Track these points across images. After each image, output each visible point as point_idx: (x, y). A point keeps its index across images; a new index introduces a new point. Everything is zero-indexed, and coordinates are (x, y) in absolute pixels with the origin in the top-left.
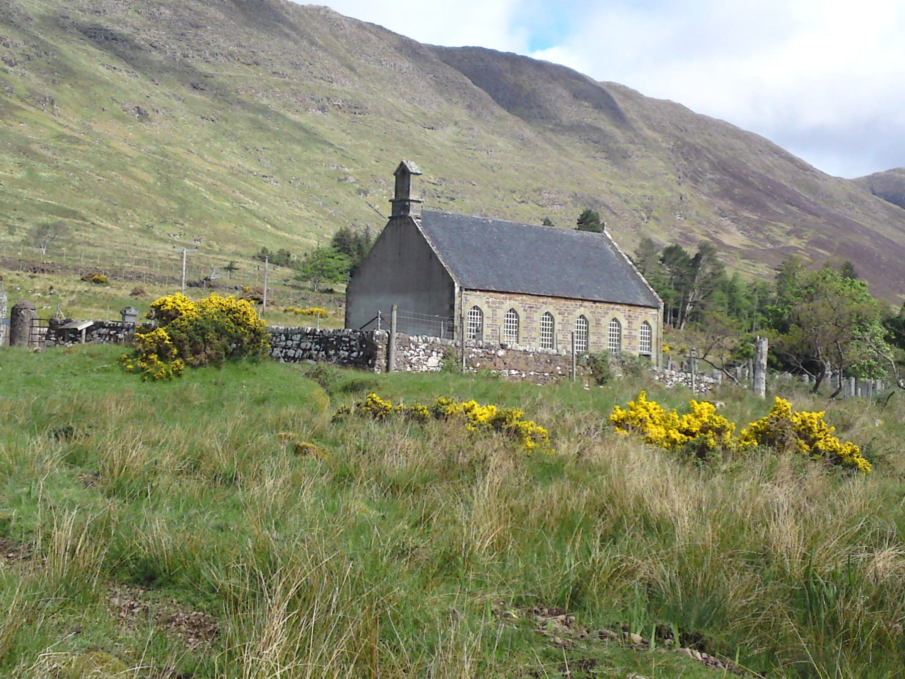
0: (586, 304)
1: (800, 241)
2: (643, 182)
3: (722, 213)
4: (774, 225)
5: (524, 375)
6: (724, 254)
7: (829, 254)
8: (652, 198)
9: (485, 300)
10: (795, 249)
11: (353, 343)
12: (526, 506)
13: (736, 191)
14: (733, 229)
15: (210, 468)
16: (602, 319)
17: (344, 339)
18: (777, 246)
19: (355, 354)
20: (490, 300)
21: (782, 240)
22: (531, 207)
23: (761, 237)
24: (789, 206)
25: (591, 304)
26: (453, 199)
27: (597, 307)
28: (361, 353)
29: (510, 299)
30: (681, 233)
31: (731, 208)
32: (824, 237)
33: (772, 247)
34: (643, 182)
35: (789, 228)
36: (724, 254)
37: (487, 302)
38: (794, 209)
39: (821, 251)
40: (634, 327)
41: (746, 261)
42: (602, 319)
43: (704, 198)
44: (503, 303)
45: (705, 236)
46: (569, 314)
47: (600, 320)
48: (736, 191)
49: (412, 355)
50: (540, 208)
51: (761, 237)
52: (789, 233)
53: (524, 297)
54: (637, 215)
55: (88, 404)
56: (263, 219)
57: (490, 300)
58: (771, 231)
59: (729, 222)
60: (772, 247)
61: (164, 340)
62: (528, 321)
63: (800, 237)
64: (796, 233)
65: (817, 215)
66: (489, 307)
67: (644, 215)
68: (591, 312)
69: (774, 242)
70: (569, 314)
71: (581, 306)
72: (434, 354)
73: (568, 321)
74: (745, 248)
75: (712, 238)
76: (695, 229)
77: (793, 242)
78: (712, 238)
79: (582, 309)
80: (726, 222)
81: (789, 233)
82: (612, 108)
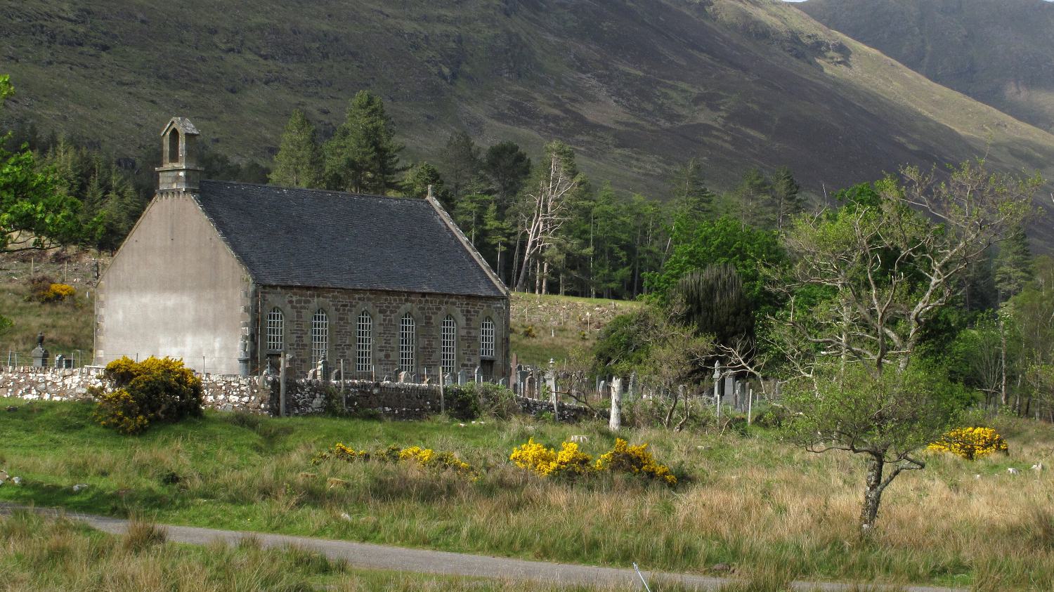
1: (715, 115)
2: (442, 12)
3: (582, 65)
4: (671, 87)
5: (397, 412)
6: (586, 138)
7: (763, 137)
8: (459, 40)
9: (287, 298)
10: (707, 129)
11: (243, 388)
13: (606, 25)
14: (603, 94)
15: (1024, 427)
17: (233, 384)
18: (678, 124)
19: (246, 399)
20: (294, 299)
21: (684, 112)
22: (248, 61)
23: (650, 107)
24: (695, 53)
26: (105, 48)
28: (253, 398)
30: (512, 102)
31: (598, 57)
32: (756, 107)
33: (668, 125)
34: (442, 12)
35: (695, 91)
36: (586, 138)
37: (291, 302)
38: (704, 57)
39: (752, 133)
41: (627, 152)
43: (551, 38)
44: (309, 302)
45: (555, 106)
47: (430, 318)
48: (606, 25)
49: (298, 398)
50: (261, 61)
51: (650, 107)
52: (697, 100)
54: (434, 70)
57: (294, 299)
58: (666, 96)
59: (594, 82)
60: (668, 125)
61: (128, 400)
62: (342, 323)
63: (715, 108)
64: (710, 101)
65: (745, 70)
66: (293, 307)
67: (446, 71)
68: (420, 309)
69: (672, 117)
70: (392, 312)
71: (407, 300)
72: (318, 395)
73: (390, 320)
74: (621, 128)
75: (567, 111)
76: (536, 95)
77: (704, 116)
78: (567, 111)
79: (409, 304)
80: (589, 81)
81: (697, 100)
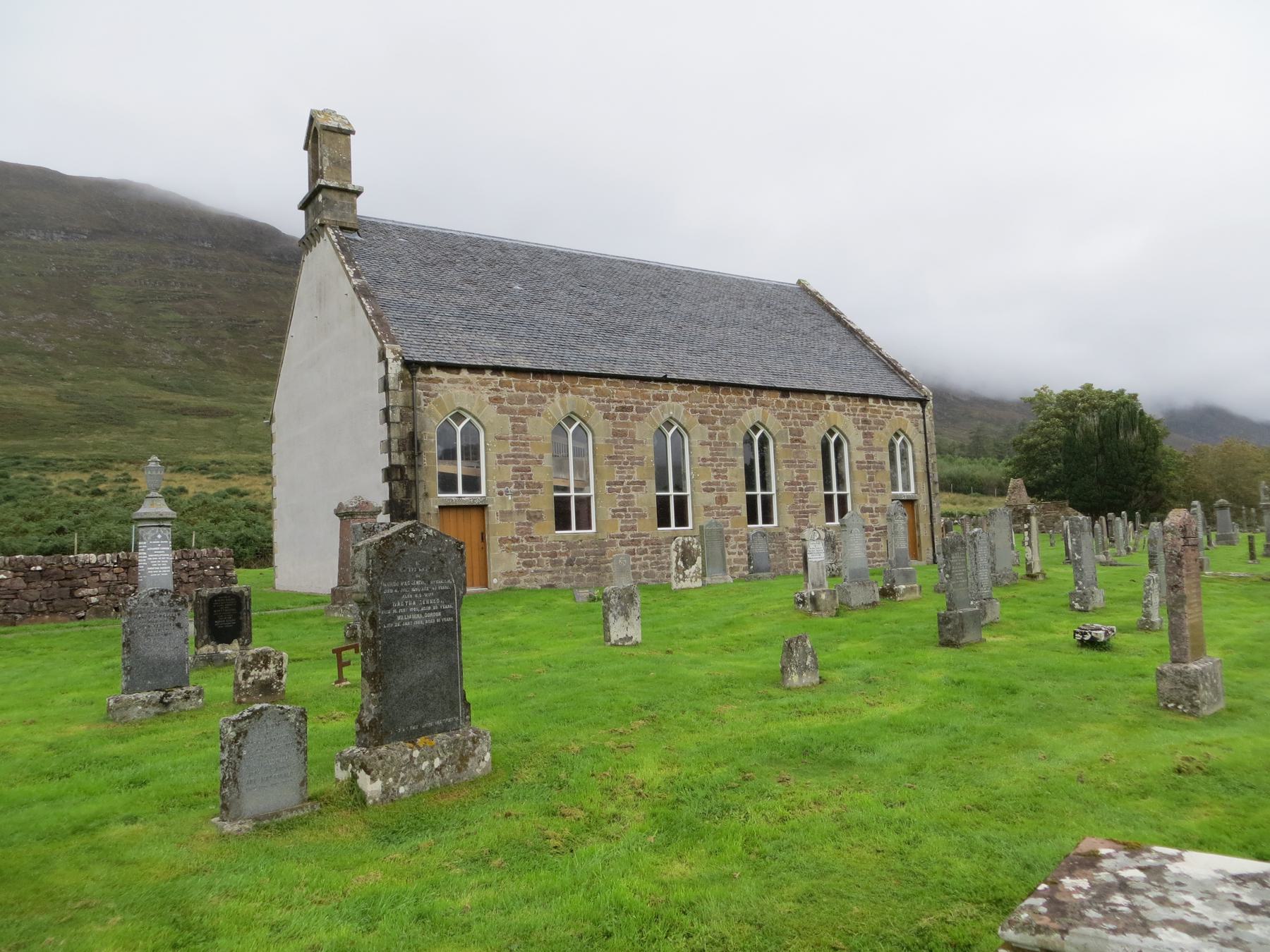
0: (765, 396)
12: (135, 863)
16: (806, 429)
20: (505, 393)
25: (777, 397)
27: (791, 404)
29: (564, 390)
40: (876, 443)
42: (806, 429)
46: (725, 421)
47: (800, 433)
53: (604, 385)
55: (624, 895)
56: (184, 411)
57: (505, 393)
68: (780, 416)
71: (753, 402)
73: (724, 436)
79: (757, 410)
82: (1201, 843)
